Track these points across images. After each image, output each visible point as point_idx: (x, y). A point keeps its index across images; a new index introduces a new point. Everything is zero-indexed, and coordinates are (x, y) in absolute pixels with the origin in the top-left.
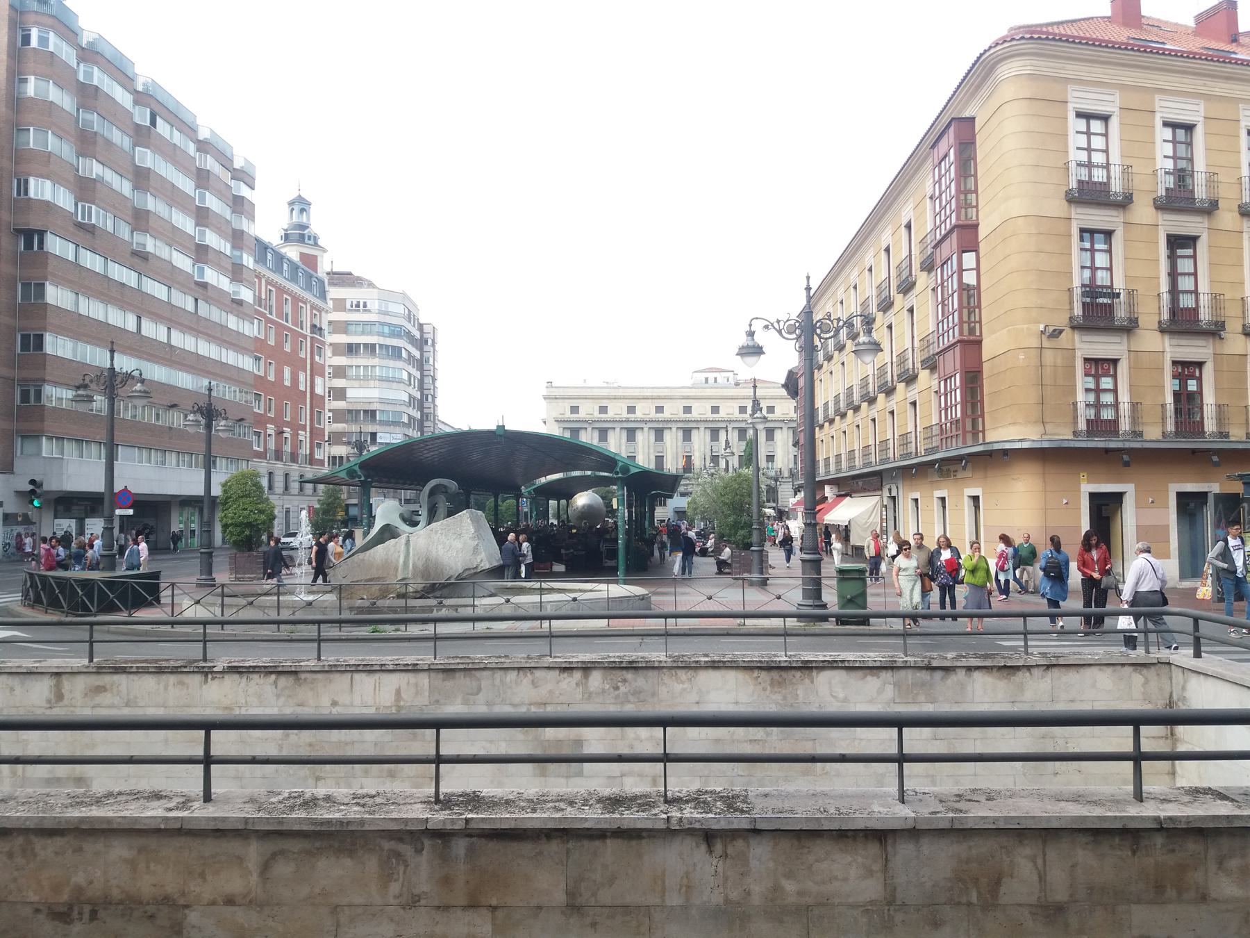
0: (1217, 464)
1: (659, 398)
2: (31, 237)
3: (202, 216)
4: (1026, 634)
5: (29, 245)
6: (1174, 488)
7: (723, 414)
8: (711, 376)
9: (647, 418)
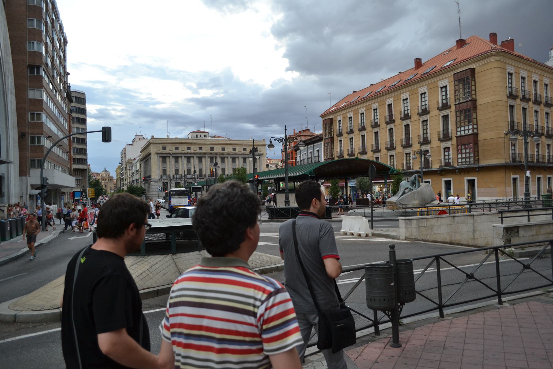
0: (477, 171)
4: (428, 211)
5: (32, 72)
6: (466, 178)
8: (199, 134)
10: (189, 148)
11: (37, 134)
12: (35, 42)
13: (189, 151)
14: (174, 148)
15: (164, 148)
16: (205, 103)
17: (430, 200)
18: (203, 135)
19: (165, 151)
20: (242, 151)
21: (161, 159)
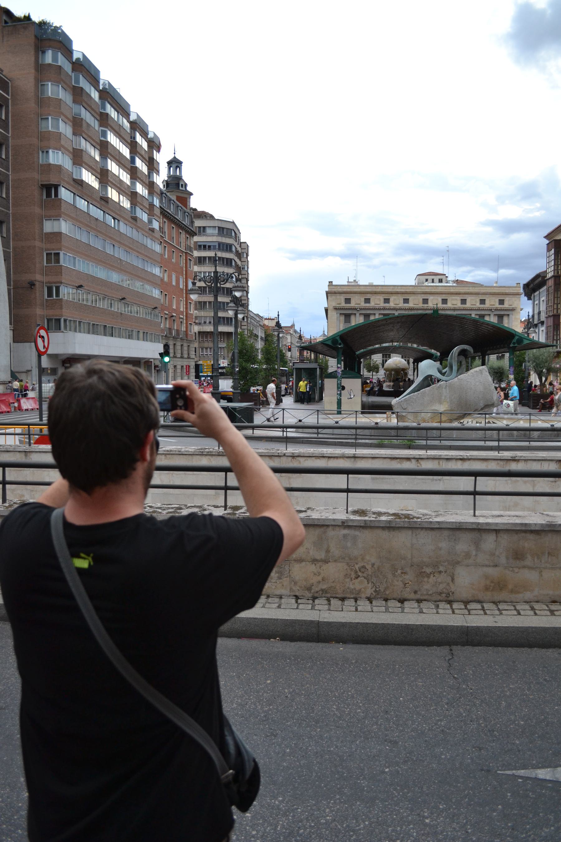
1: (406, 293)
2: (50, 189)
3: (134, 172)
4: (356, 435)
5: (49, 195)
7: (468, 305)
9: (398, 307)
10: (387, 301)
11: (55, 283)
12: (50, 151)
13: (387, 305)
14: (363, 299)
15: (348, 301)
16: (510, 227)
17: (482, 405)
18: (436, 278)
19: (387, 305)
20: (478, 305)
21: (342, 318)
